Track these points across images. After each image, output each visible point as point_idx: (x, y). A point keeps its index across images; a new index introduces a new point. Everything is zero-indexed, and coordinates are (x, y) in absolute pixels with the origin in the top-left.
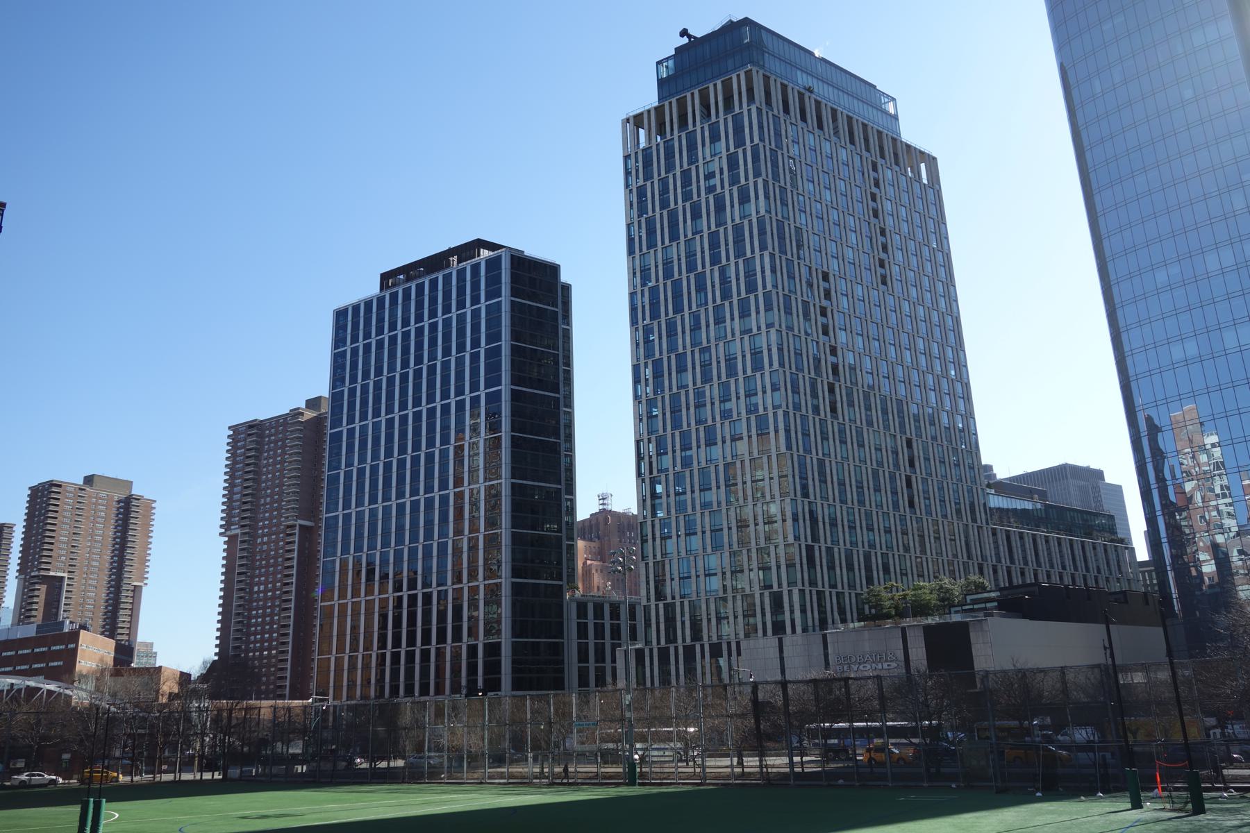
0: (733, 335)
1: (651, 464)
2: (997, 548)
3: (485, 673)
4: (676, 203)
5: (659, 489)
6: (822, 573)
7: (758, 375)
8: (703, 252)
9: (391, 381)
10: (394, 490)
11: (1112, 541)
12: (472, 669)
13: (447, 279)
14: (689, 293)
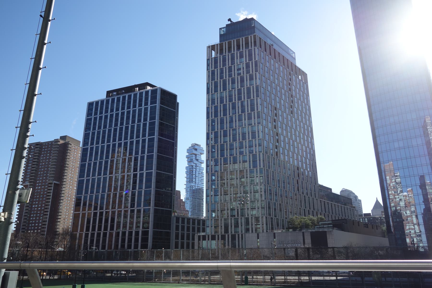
0: (245, 125)
1: (212, 168)
2: (321, 207)
3: (142, 242)
4: (226, 77)
5: (213, 178)
6: (272, 211)
7: (254, 140)
8: (235, 95)
9: (110, 131)
10: (108, 171)
11: (352, 207)
12: (137, 240)
13: (135, 95)
14: (229, 109)
